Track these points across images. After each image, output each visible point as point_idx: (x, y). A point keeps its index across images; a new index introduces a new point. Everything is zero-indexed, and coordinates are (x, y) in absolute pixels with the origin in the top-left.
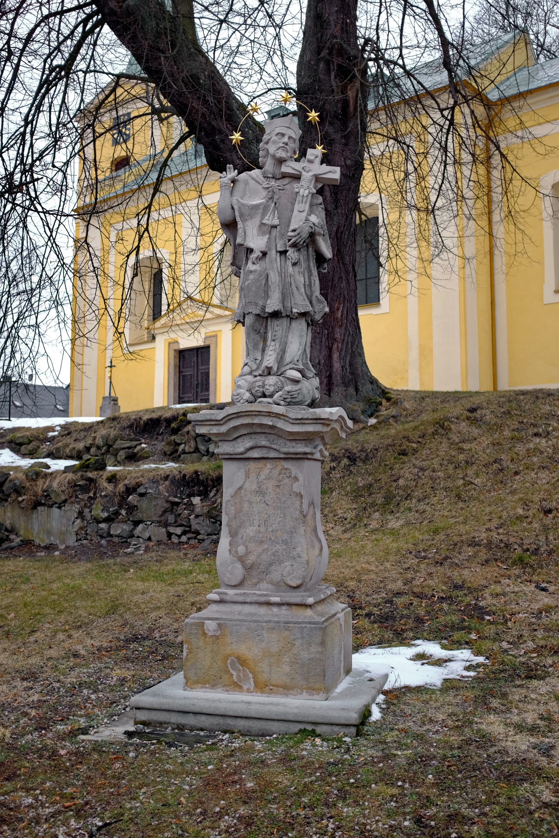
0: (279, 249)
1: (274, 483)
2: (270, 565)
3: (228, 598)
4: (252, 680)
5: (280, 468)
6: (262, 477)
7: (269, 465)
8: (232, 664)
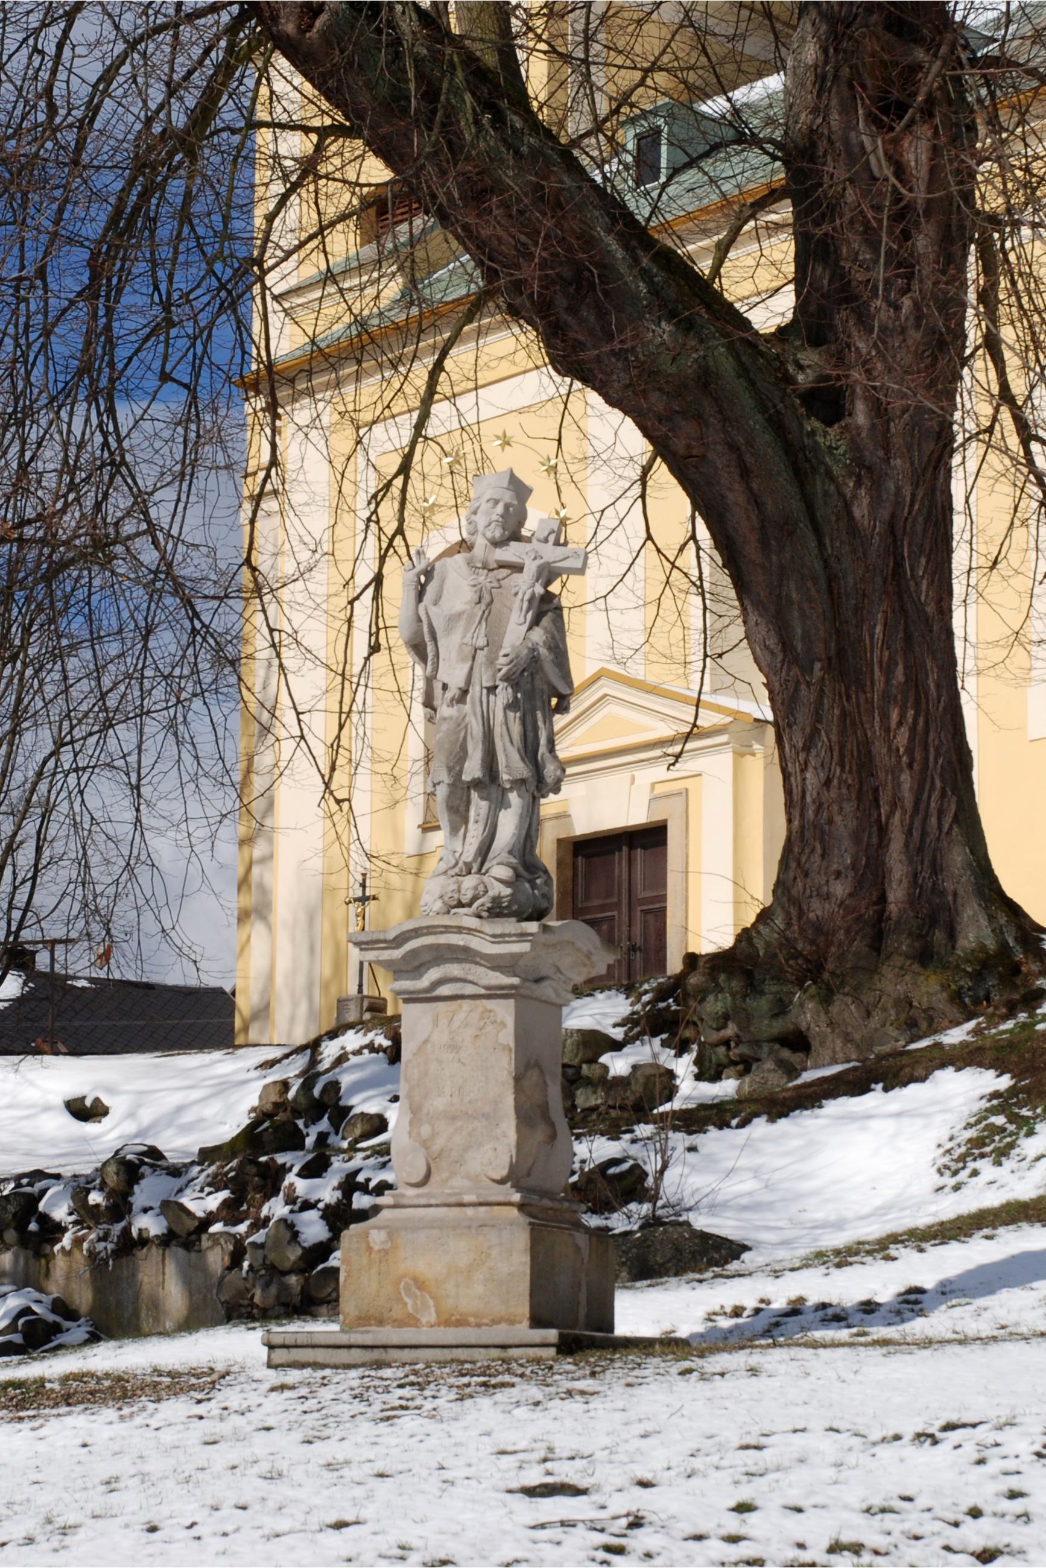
0: (485, 684)
1: (470, 1032)
2: (466, 1149)
3: (405, 1201)
4: (433, 1310)
5: (480, 1009)
6: (456, 1023)
7: (466, 1004)
8: (407, 1289)
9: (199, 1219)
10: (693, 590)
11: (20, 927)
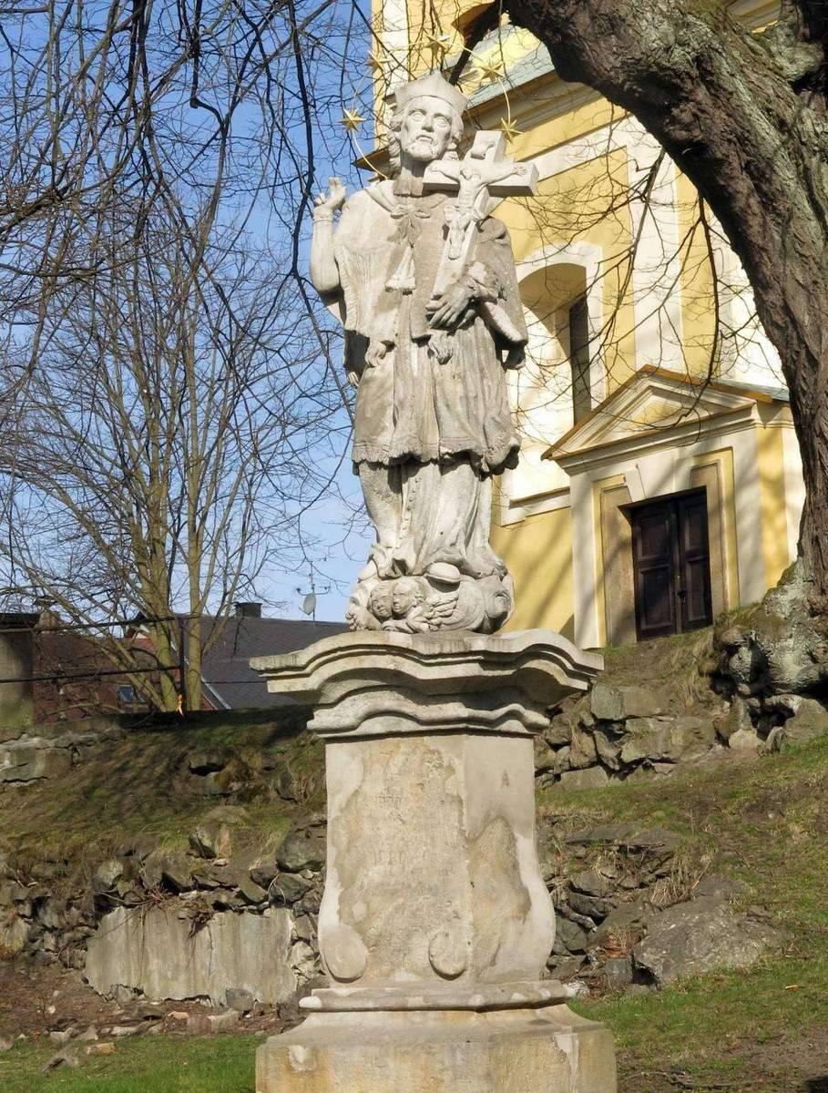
3: (337, 1004)
6: (394, 770)
9: (728, 738)
10: (16, 49)
11: (234, 588)
